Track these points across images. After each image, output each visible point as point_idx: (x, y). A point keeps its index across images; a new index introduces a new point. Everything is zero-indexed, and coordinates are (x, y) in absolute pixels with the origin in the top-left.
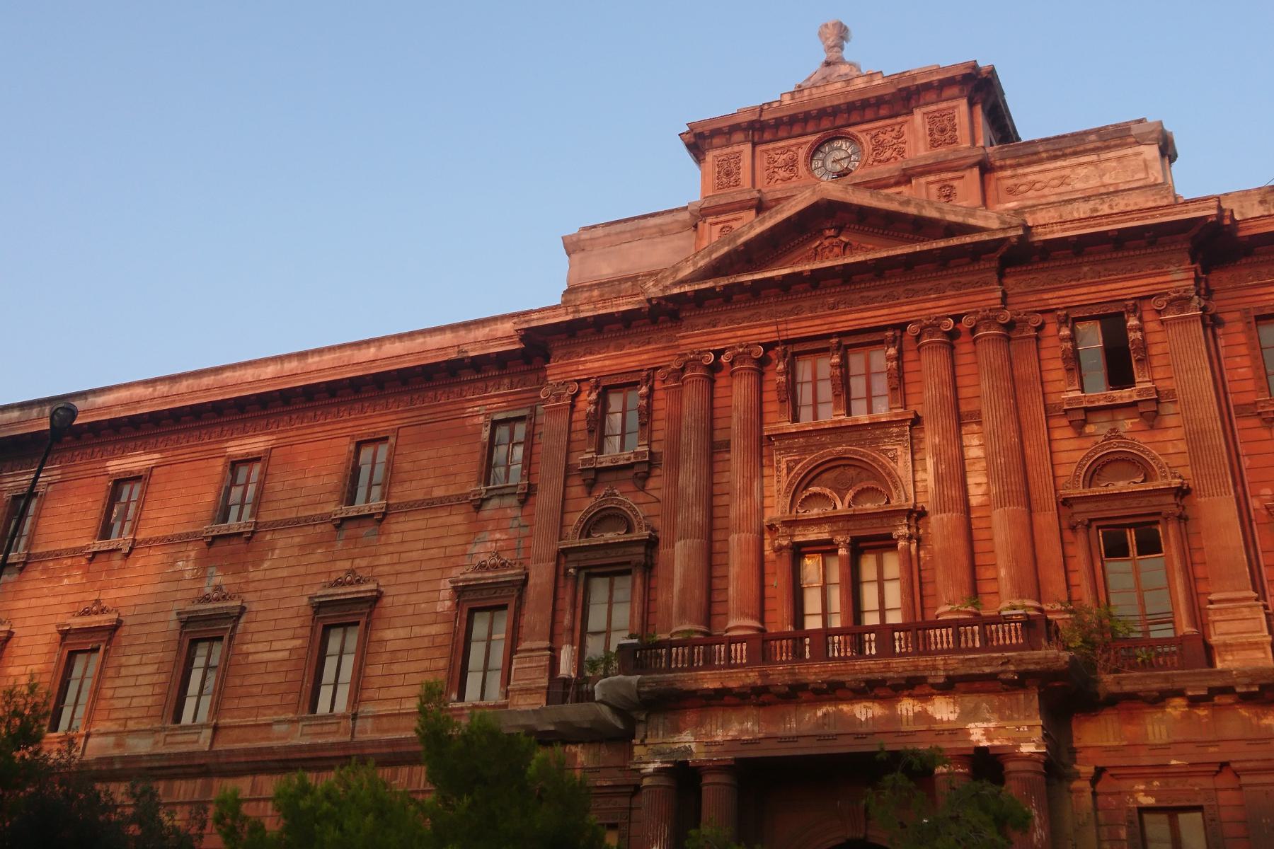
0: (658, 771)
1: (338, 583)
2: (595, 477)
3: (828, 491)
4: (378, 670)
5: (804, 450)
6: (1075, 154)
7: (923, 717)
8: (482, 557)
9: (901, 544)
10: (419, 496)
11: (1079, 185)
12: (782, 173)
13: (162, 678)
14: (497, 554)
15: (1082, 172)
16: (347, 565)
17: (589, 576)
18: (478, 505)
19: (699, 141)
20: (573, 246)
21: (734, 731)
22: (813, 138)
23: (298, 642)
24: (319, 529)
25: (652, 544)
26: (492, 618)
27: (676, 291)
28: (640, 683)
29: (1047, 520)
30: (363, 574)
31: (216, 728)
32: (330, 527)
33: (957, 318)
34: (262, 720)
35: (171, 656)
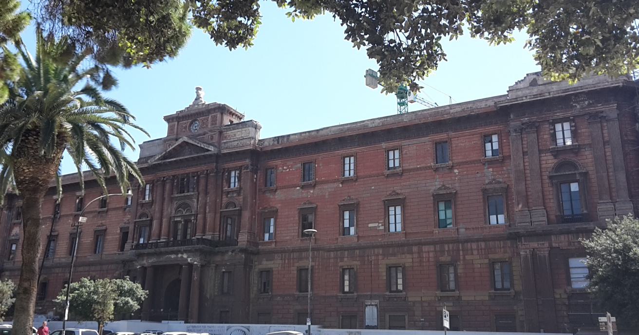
0: (140, 268)
1: (99, 226)
2: (143, 205)
3: (182, 209)
4: (107, 245)
5: (179, 200)
6: (238, 129)
7: (182, 257)
8: (125, 221)
9: (193, 221)
10: (114, 207)
11: (237, 137)
12: (184, 130)
13: (67, 246)
14: (128, 220)
15: (239, 133)
16: (101, 222)
17: (560, 184)
18: (125, 209)
19: (168, 119)
20: (509, 87)
21: (152, 260)
22: (190, 121)
23: (82, 240)
24: (95, 214)
25: (240, 211)
26: (567, 192)
27: (154, 163)
28: (135, 252)
29: (218, 215)
30: (104, 224)
31: (77, 257)
32: (97, 213)
33: (207, 171)
34: (86, 255)
35: (68, 241)
